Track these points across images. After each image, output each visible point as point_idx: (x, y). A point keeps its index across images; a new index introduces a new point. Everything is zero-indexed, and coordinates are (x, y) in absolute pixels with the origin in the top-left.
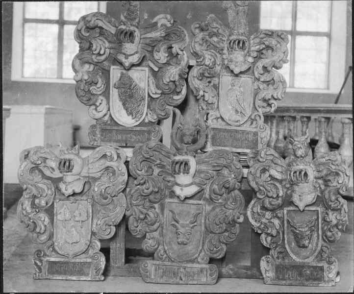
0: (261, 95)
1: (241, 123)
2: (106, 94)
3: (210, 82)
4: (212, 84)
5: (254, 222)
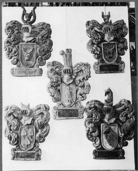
0: (78, 93)
1: (71, 106)
2: (99, 136)
3: (56, 89)
4: (57, 89)
5: (79, 78)
